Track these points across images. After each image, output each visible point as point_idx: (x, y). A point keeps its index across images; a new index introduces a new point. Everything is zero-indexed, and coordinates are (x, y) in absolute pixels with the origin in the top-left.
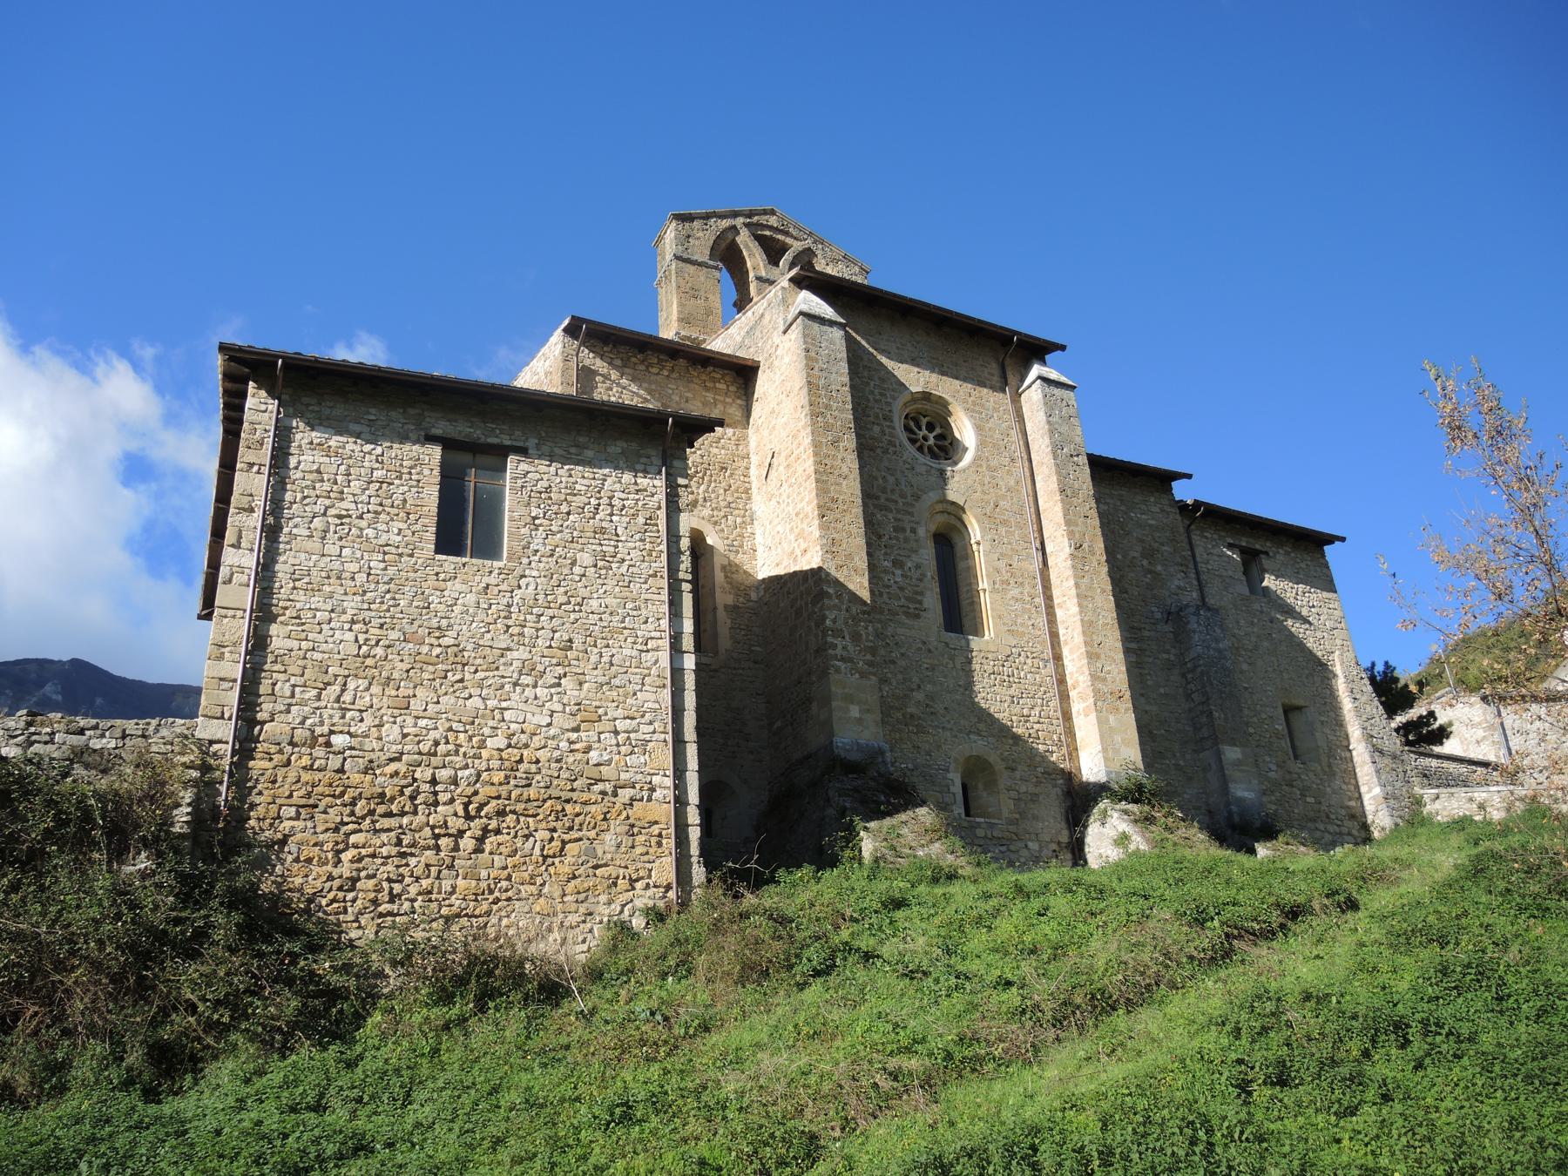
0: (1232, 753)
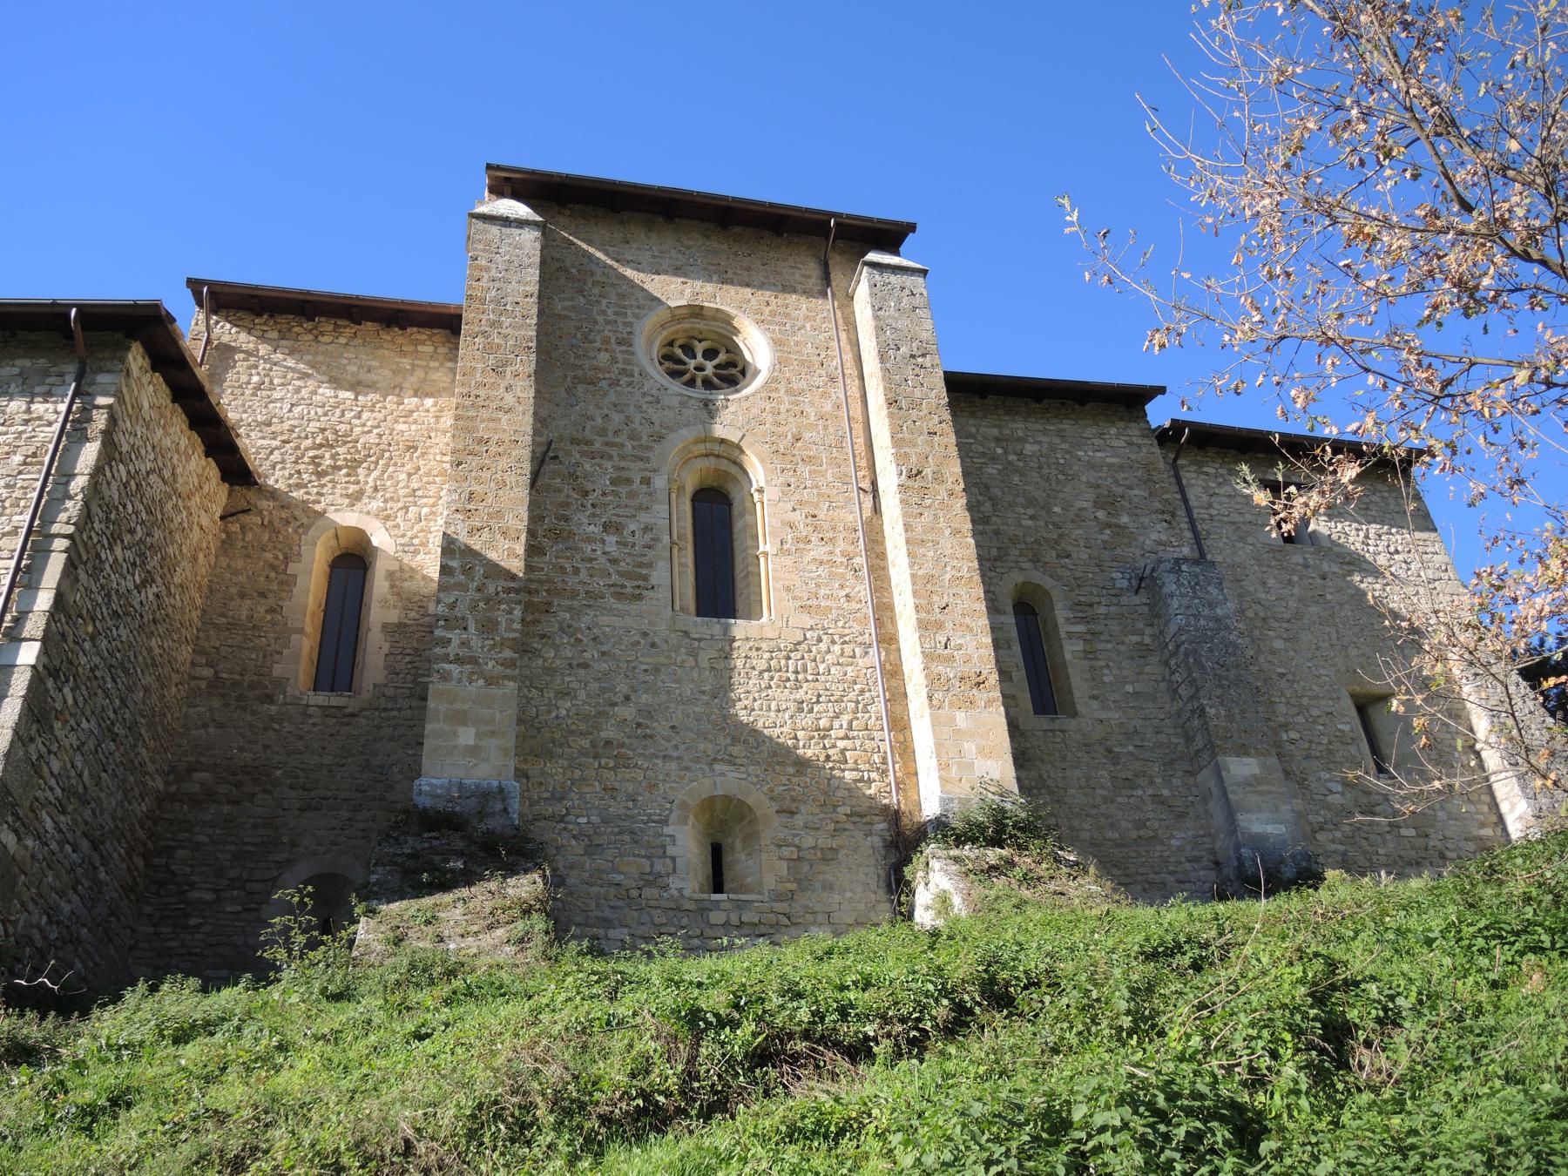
0: (1240, 768)
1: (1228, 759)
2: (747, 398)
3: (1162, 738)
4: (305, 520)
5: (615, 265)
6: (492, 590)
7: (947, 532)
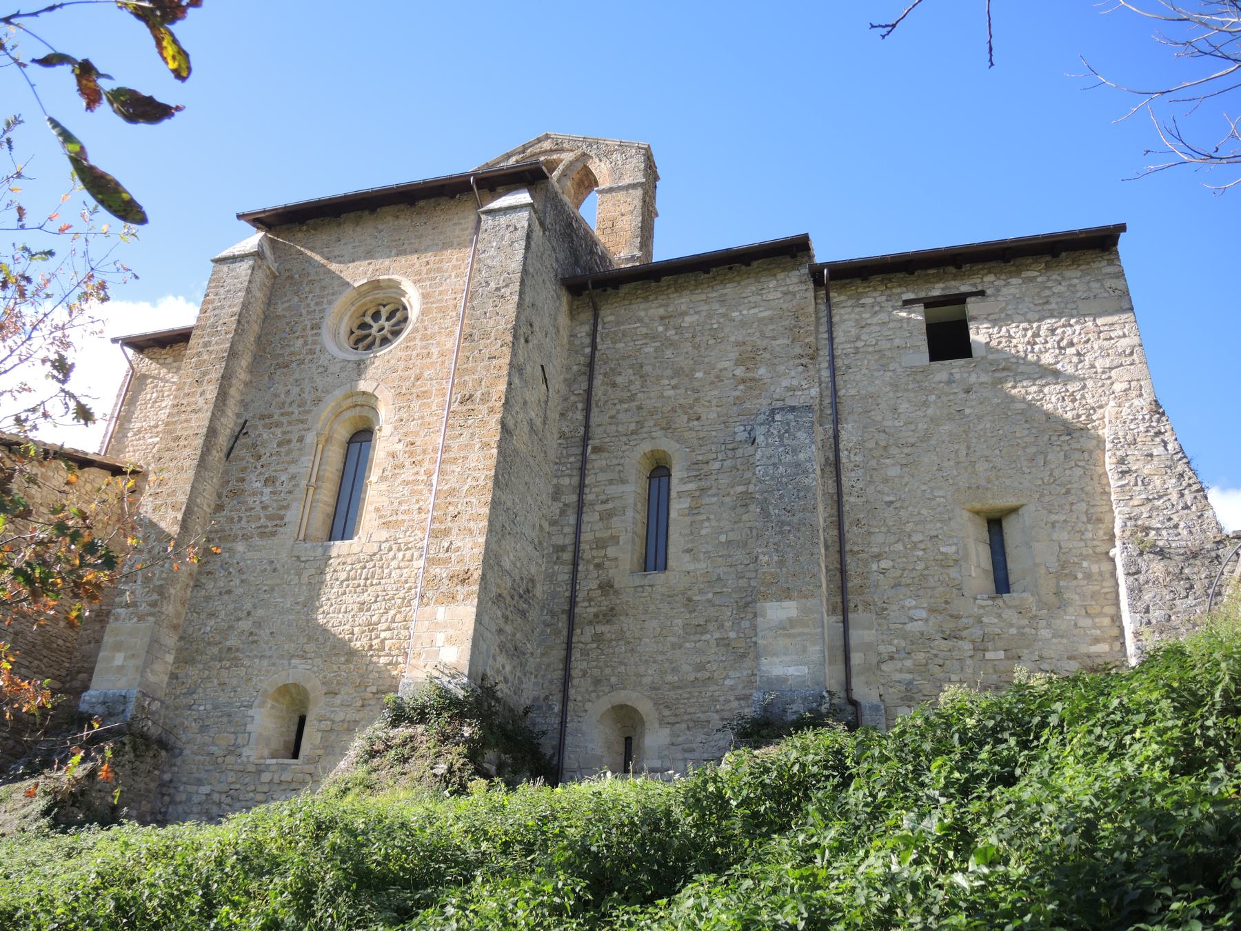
1: (768, 604)
3: (742, 583)
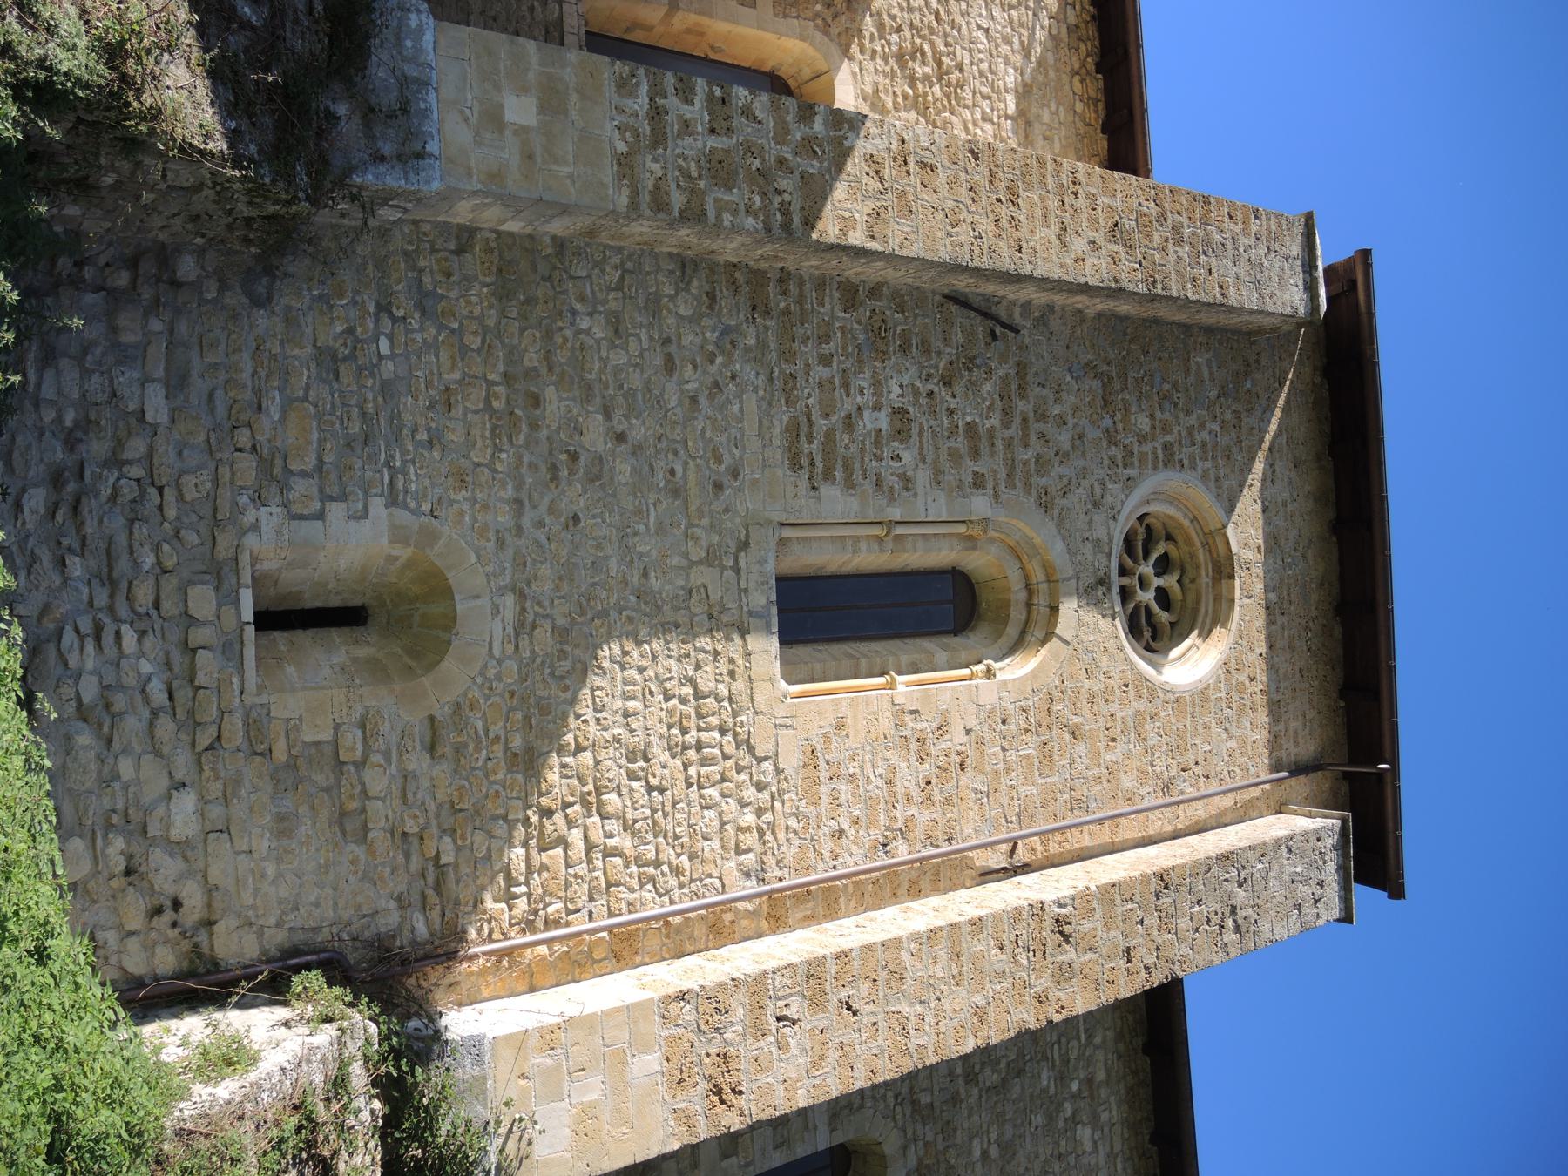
2: (1121, 649)
4: (834, 30)
5: (1266, 446)
6: (784, 183)
7: (979, 999)
